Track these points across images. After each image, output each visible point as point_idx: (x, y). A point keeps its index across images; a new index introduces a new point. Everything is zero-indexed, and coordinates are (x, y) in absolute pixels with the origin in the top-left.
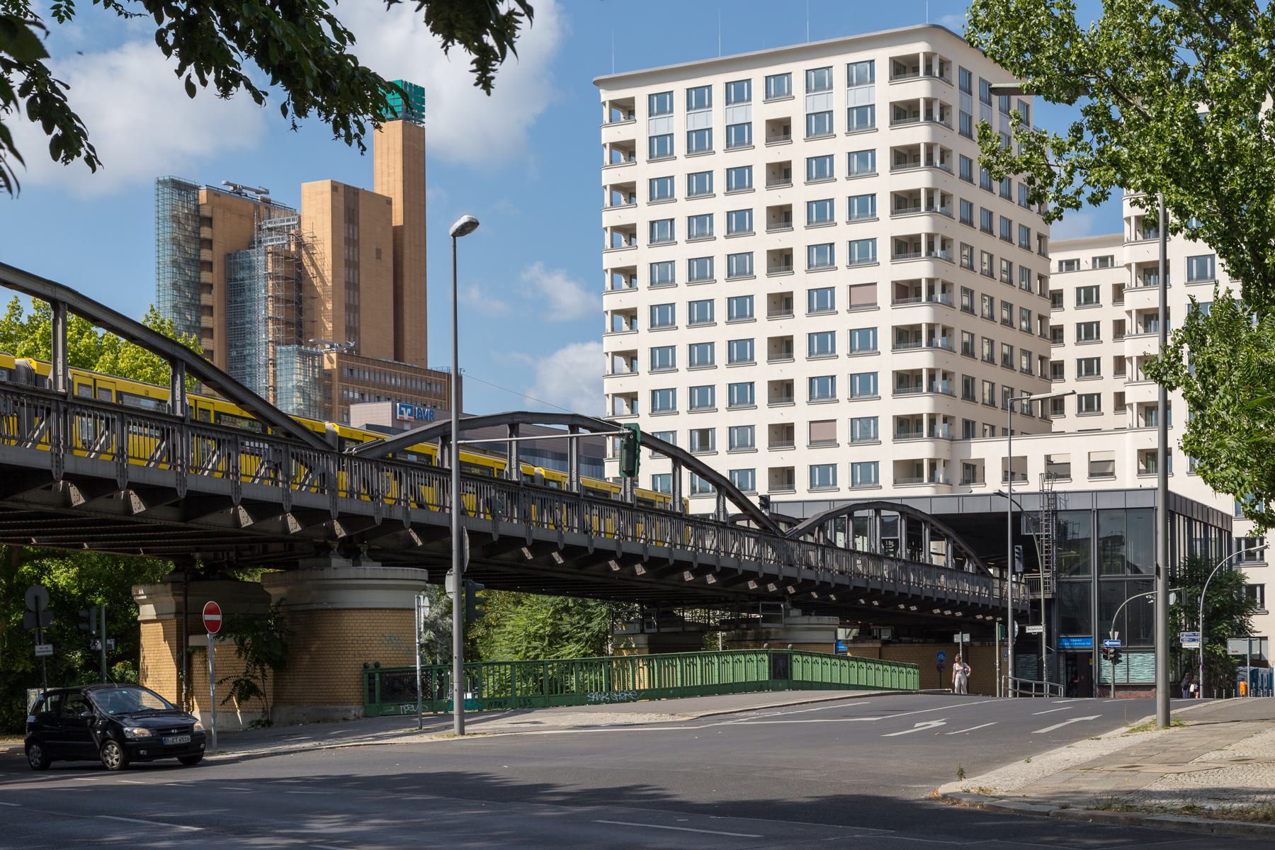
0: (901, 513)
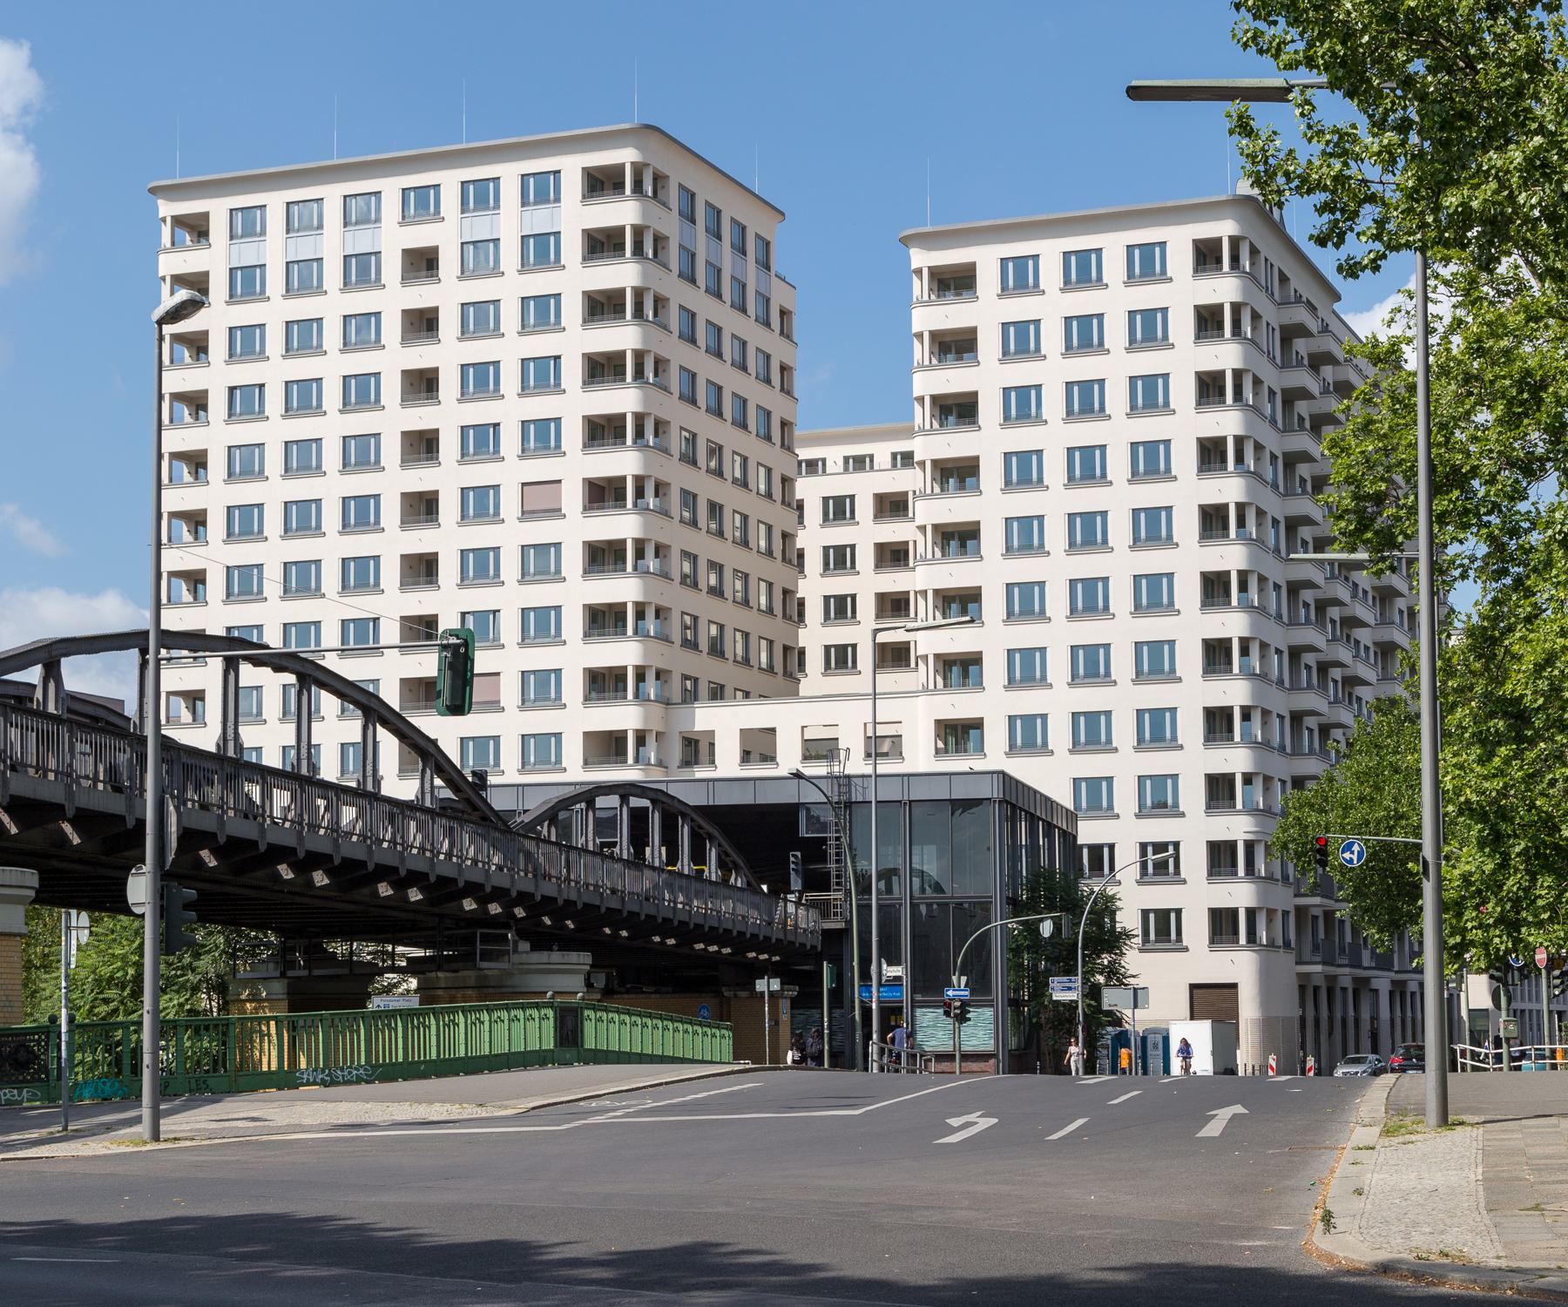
0: (653, 801)
